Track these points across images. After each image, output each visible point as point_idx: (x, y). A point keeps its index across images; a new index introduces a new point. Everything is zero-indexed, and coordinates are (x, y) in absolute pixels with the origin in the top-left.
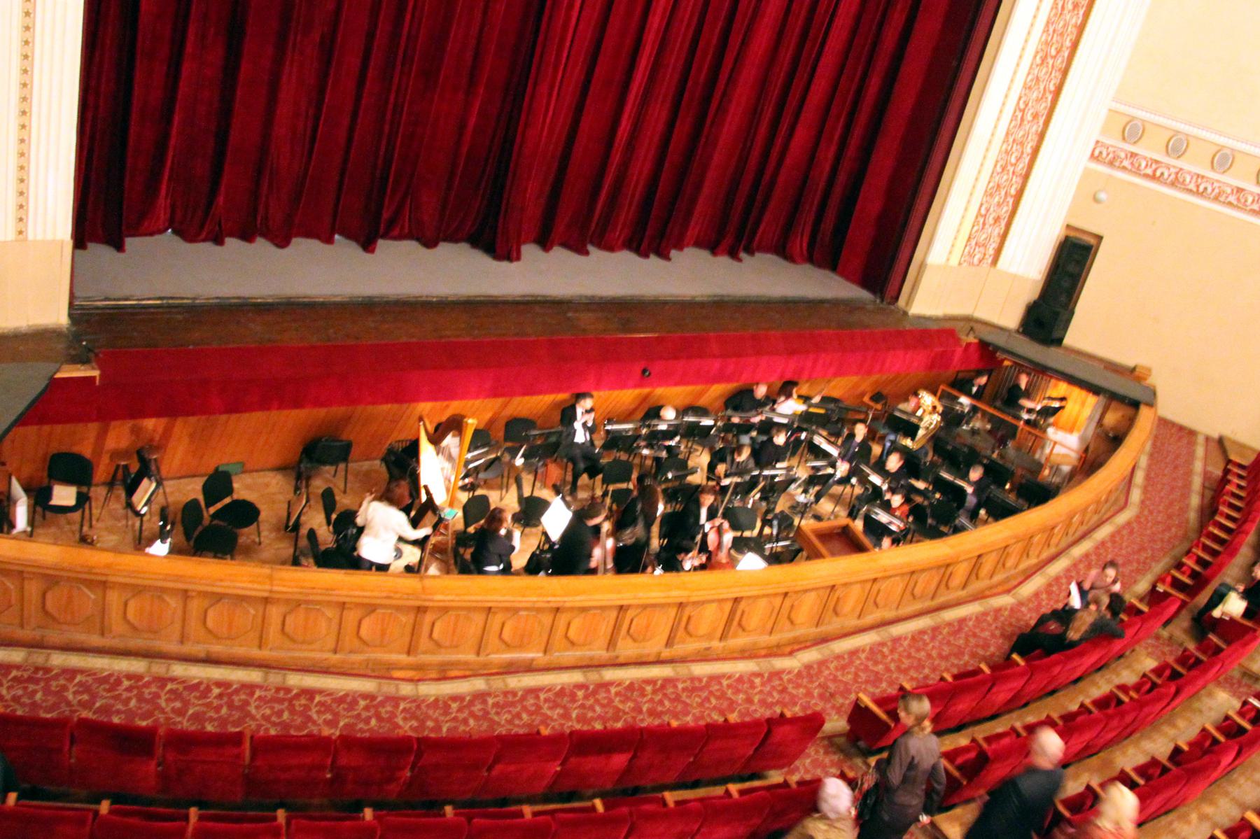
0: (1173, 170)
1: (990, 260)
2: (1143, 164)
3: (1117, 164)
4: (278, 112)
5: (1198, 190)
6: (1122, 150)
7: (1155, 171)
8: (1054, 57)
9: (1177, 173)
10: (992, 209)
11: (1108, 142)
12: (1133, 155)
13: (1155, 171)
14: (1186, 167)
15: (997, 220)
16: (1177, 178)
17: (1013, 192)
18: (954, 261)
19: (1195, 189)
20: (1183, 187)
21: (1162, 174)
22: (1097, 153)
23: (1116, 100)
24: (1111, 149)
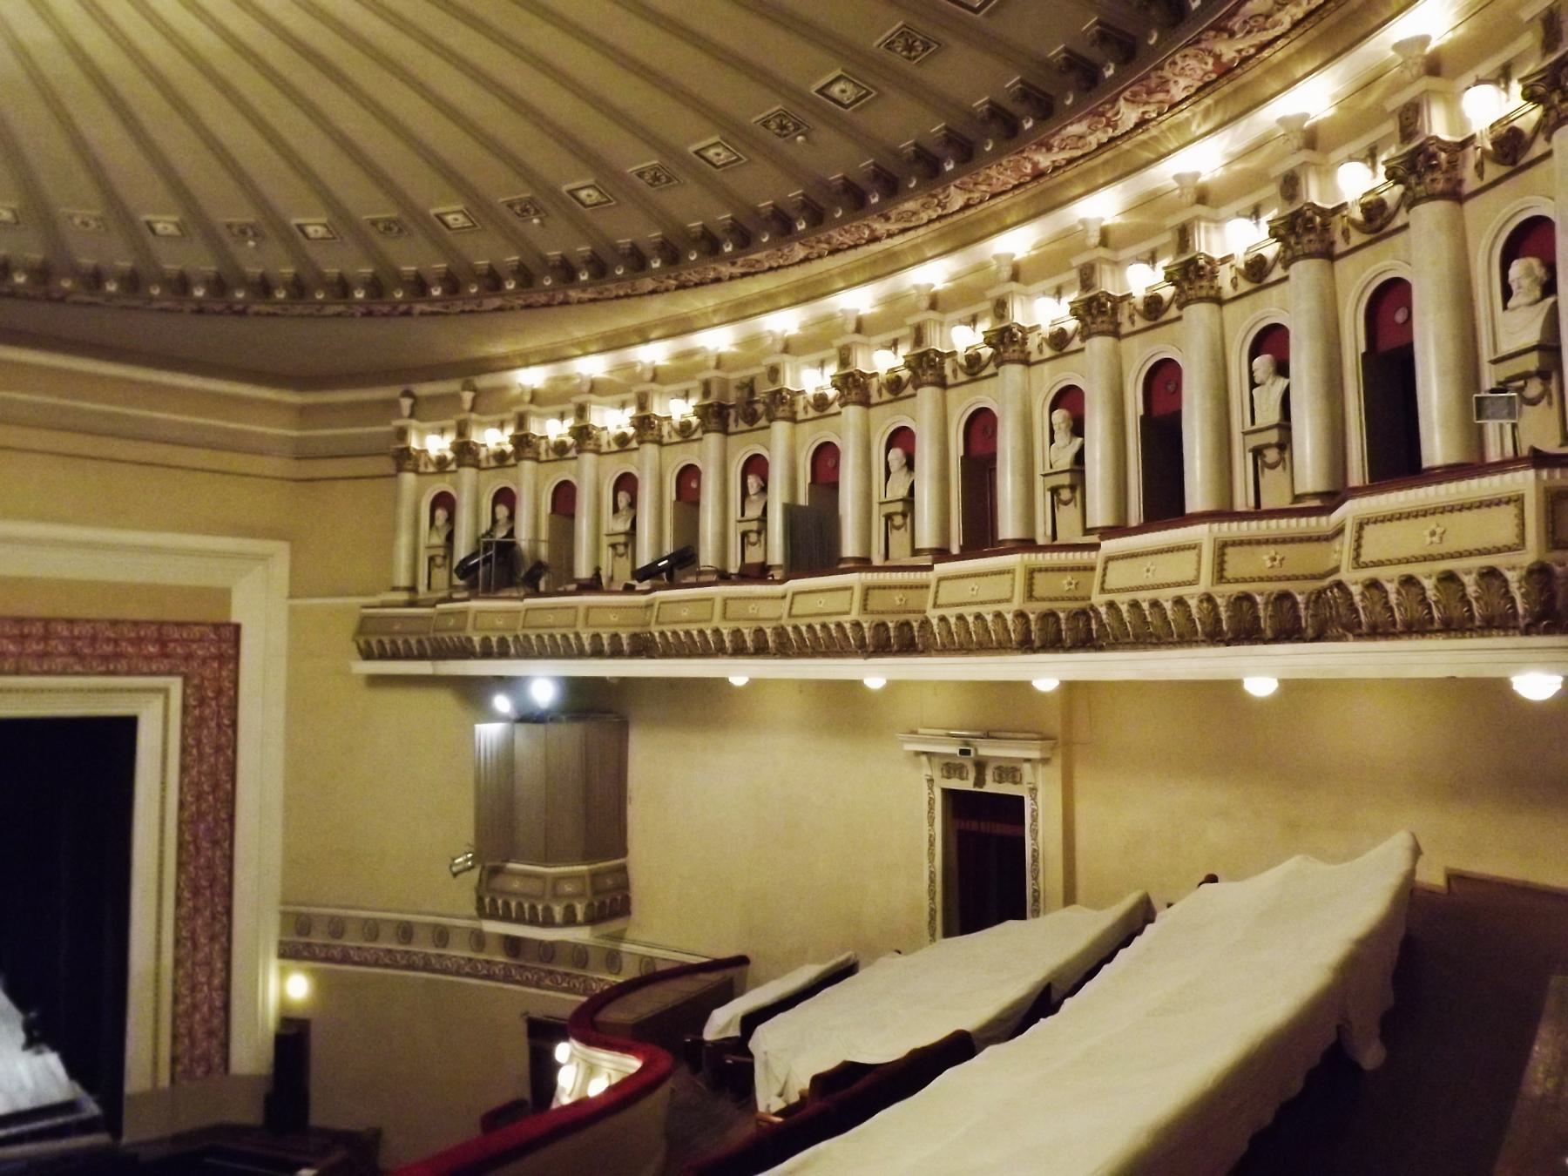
1: (221, 1070)
14: (348, 944)
17: (218, 1003)
18: (164, 1080)
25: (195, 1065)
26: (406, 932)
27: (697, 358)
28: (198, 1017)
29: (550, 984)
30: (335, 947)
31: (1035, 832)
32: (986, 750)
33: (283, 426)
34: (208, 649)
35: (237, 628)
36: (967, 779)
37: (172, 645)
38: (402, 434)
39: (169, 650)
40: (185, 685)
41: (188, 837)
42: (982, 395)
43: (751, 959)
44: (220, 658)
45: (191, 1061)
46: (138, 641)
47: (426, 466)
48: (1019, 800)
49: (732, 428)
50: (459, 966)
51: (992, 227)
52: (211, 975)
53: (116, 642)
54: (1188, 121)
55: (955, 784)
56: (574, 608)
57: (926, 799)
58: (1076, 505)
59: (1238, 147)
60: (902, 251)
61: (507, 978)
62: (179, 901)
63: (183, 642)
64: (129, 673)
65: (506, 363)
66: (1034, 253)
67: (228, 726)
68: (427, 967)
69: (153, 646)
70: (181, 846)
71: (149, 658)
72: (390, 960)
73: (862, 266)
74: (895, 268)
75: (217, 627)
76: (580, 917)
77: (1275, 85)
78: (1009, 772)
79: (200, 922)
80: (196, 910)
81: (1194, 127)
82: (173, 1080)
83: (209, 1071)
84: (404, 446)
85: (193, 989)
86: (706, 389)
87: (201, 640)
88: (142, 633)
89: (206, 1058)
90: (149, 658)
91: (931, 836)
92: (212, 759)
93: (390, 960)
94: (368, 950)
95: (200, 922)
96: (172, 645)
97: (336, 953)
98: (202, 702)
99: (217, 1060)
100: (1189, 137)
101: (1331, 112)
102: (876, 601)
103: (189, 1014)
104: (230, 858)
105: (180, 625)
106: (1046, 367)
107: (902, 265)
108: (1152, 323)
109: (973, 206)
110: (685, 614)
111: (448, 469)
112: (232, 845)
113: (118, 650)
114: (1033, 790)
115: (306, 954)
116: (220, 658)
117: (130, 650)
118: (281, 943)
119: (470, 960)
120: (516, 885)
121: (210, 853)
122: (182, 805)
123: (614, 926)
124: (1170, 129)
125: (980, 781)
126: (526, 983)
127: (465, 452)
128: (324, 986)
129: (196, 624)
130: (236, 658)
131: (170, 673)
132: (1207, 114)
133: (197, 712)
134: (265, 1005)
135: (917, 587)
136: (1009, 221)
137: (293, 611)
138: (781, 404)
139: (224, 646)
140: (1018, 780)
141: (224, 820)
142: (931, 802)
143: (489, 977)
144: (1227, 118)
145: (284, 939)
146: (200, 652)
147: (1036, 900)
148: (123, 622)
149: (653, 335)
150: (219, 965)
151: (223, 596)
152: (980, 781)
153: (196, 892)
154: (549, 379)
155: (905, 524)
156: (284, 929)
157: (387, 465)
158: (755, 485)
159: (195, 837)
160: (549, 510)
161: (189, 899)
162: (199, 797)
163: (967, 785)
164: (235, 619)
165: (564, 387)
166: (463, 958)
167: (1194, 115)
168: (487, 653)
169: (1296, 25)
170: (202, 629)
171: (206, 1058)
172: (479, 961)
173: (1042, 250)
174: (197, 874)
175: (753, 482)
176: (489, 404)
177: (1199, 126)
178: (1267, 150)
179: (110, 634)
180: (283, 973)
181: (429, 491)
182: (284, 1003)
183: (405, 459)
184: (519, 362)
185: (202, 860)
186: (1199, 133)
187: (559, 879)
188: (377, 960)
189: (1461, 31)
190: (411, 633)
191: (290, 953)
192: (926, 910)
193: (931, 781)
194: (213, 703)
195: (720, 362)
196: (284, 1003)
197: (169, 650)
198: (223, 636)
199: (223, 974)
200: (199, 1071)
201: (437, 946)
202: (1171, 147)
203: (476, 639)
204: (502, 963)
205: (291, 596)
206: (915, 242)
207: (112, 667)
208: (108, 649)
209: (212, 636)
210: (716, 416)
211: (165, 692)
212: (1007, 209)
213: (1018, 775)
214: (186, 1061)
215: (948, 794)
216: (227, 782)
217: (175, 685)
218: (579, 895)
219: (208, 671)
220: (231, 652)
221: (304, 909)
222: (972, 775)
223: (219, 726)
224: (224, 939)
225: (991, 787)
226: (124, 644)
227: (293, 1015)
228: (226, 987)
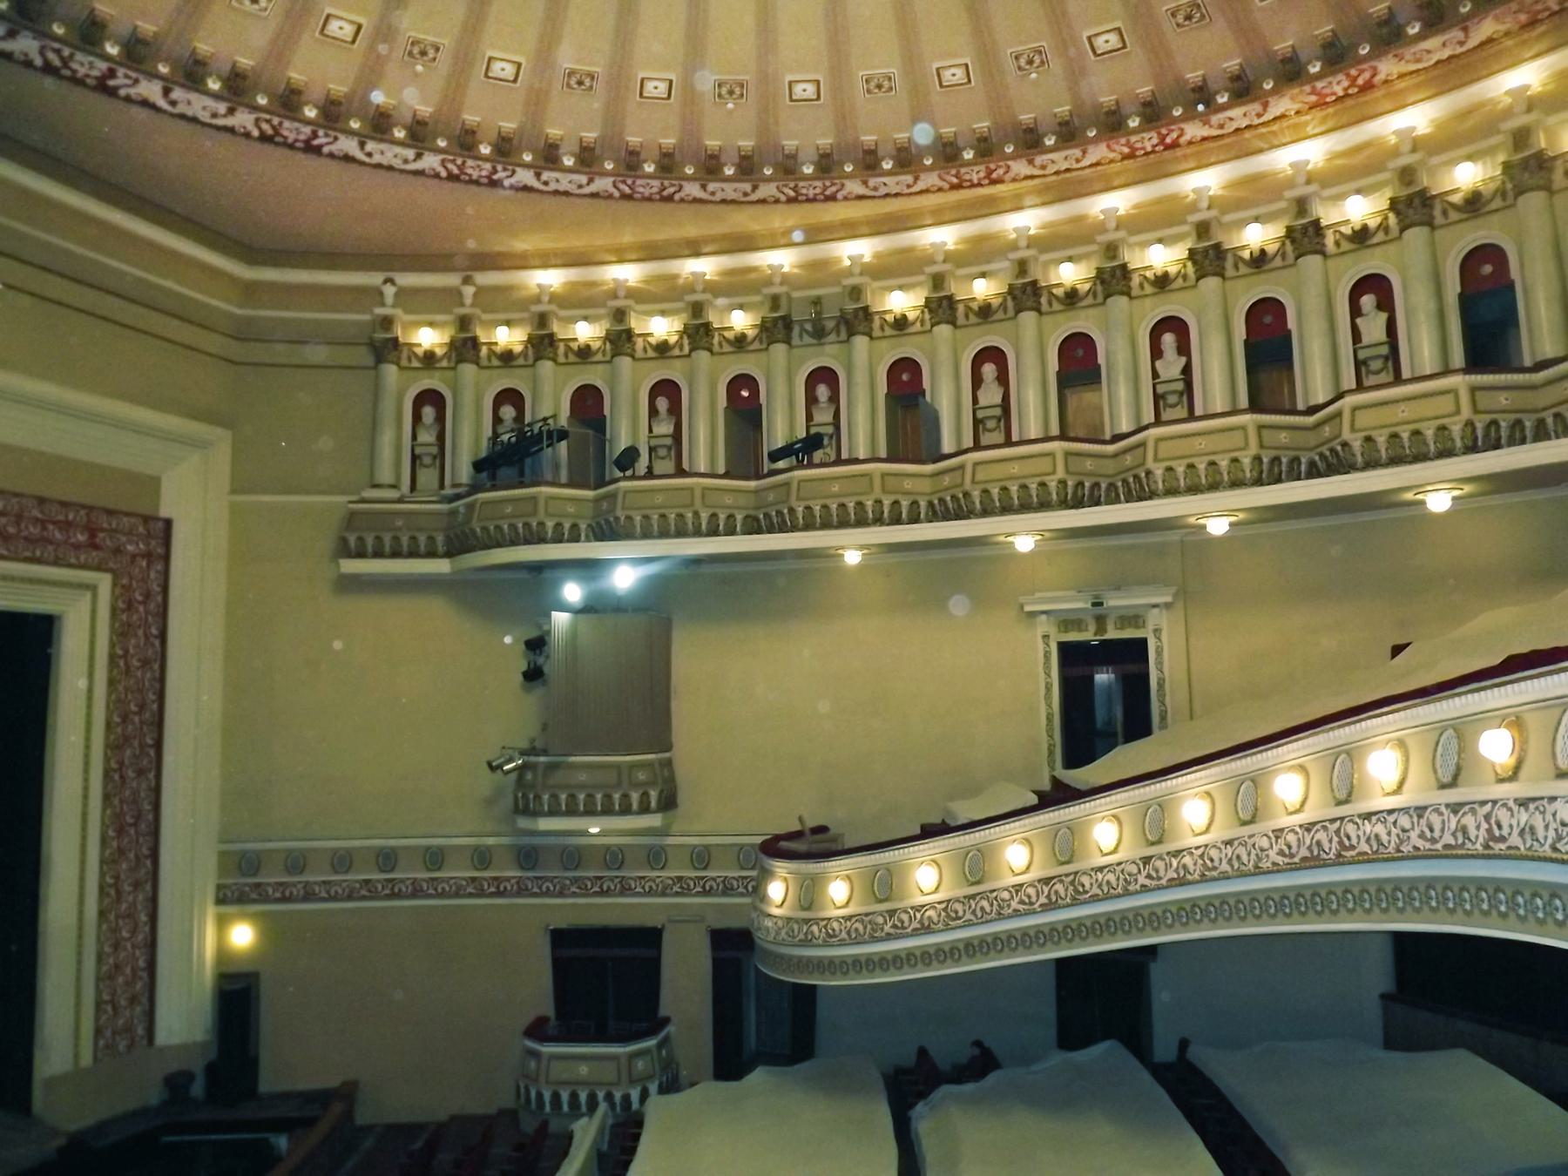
0: (300, 886)
1: (145, 1042)
2: (380, 887)
3: (355, 895)
4: (356, 69)
5: (748, 891)
6: (567, 878)
7: (392, 889)
8: (135, 825)
9: (518, 883)
10: (119, 992)
11: (230, 881)
12: (258, 885)
13: (601, 887)
14: (311, 879)
15: (133, 1000)
16: (622, 886)
17: (141, 963)
18: (86, 1059)
19: (326, 895)
20: (526, 892)
21: (505, 888)
22: (221, 895)
23: (222, 841)
24: (718, 880)
25: (118, 1038)
26: (387, 859)
27: (753, 276)
28: (121, 980)
29: (577, 890)
30: (294, 885)
31: (1159, 664)
32: (1114, 601)
33: (228, 300)
34: (138, 544)
35: (168, 523)
36: (1087, 630)
37: (101, 535)
38: (387, 322)
39: (97, 540)
40: (114, 585)
41: (114, 765)
42: (1082, 322)
43: (829, 826)
44: (148, 555)
45: (114, 1033)
46: (67, 526)
47: (410, 360)
48: (1143, 642)
49: (796, 341)
50: (459, 888)
51: (1098, 186)
52: (134, 932)
53: (43, 523)
54: (1306, 124)
55: (1073, 636)
56: (691, 489)
57: (1041, 654)
58: (1183, 407)
59: (1340, 147)
60: (1002, 198)
61: (522, 891)
62: (104, 841)
63: (113, 532)
64: (56, 563)
65: (523, 262)
66: (1132, 212)
67: (156, 637)
68: (417, 892)
69: (82, 534)
70: (107, 774)
71: (77, 547)
72: (369, 890)
73: (958, 206)
74: (989, 211)
75: (147, 519)
76: (653, 804)
77: (1388, 106)
78: (1135, 619)
79: (124, 866)
80: (121, 851)
81: (1309, 129)
82: (95, 1058)
83: (131, 1046)
84: (389, 336)
85: (116, 946)
86: (775, 301)
87: (129, 533)
88: (71, 517)
89: (129, 1029)
90: (77, 547)
91: (1047, 683)
92: (139, 674)
93: (369, 890)
94: (339, 883)
95: (124, 866)
96: (101, 535)
97: (298, 891)
98: (130, 605)
99: (140, 1031)
100: (1302, 135)
101: (1428, 131)
102: (1076, 464)
103: (111, 977)
104: (157, 790)
105: (110, 512)
106: (1148, 301)
107: (1000, 210)
108: (898, 332)
109: (1102, 165)
110: (836, 489)
111: (438, 365)
112: (158, 776)
113: (45, 533)
114: (1157, 632)
115: (254, 896)
116: (148, 555)
117: (58, 535)
118: (219, 887)
119: (474, 879)
120: (582, 777)
121: (134, 784)
122: (109, 726)
123: (670, 814)
124: (1288, 127)
125: (1101, 629)
126: (547, 894)
127: (465, 348)
128: (270, 930)
129: (127, 514)
130: (166, 558)
131: (98, 568)
132: (1324, 119)
133: (124, 617)
134: (201, 956)
135: (1204, 434)
136: (1116, 183)
137: (235, 510)
138: (858, 320)
139: (153, 543)
140: (1141, 624)
141: (150, 746)
142: (1047, 655)
143: (499, 894)
144: (1340, 124)
145: (224, 881)
146: (130, 548)
147: (1163, 718)
148: (51, 501)
149: (706, 250)
150: (143, 918)
151: (152, 485)
152: (1101, 629)
153: (120, 831)
154: (566, 284)
155: (999, 427)
156: (223, 870)
157: (363, 356)
158: (825, 393)
159: (121, 763)
160: (568, 414)
161: (113, 838)
162: (125, 718)
163: (1088, 635)
164: (164, 512)
165: (586, 293)
166: (357, 881)
167: (1313, 119)
168: (558, 539)
169: (1438, 62)
170: (133, 520)
171: (129, 1029)
172: (484, 879)
173: (1142, 210)
174: (122, 809)
175: (822, 391)
176: (505, 304)
177: (1314, 128)
178: (1366, 153)
179: (36, 513)
180: (222, 923)
181: (411, 389)
182: (223, 953)
183: (386, 349)
184: (537, 262)
185: (127, 793)
186: (1311, 133)
187: (633, 766)
188: (351, 892)
189: (1549, 87)
190: (420, 530)
191: (231, 898)
192: (1045, 746)
193: (1046, 637)
194: (141, 609)
195: (786, 279)
196: (223, 953)
197: (97, 540)
198: (152, 532)
199: (147, 929)
200: (122, 1045)
201: (429, 870)
202: (1284, 141)
203: (550, 524)
204: (514, 877)
205: (233, 491)
206: (1018, 191)
207: (38, 553)
208: (35, 530)
209: (141, 529)
210: (777, 328)
211: (93, 588)
212: (1118, 174)
213: (1141, 621)
214: (108, 1033)
215: (1064, 648)
216: (153, 702)
217: (104, 582)
218: (651, 783)
219: (137, 570)
220: (160, 550)
221: (249, 846)
222: (1092, 628)
223: (146, 637)
224: (148, 887)
225: (1112, 634)
226: (51, 527)
227: (232, 969)
228: (152, 945)
